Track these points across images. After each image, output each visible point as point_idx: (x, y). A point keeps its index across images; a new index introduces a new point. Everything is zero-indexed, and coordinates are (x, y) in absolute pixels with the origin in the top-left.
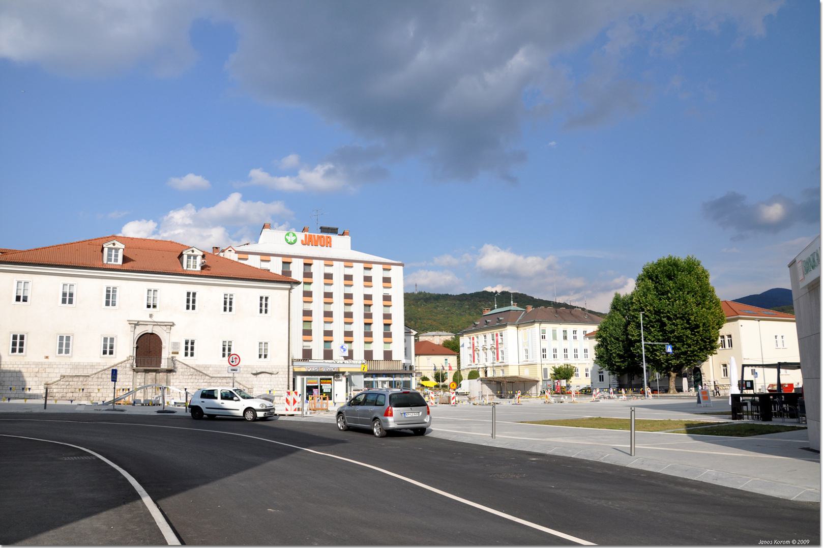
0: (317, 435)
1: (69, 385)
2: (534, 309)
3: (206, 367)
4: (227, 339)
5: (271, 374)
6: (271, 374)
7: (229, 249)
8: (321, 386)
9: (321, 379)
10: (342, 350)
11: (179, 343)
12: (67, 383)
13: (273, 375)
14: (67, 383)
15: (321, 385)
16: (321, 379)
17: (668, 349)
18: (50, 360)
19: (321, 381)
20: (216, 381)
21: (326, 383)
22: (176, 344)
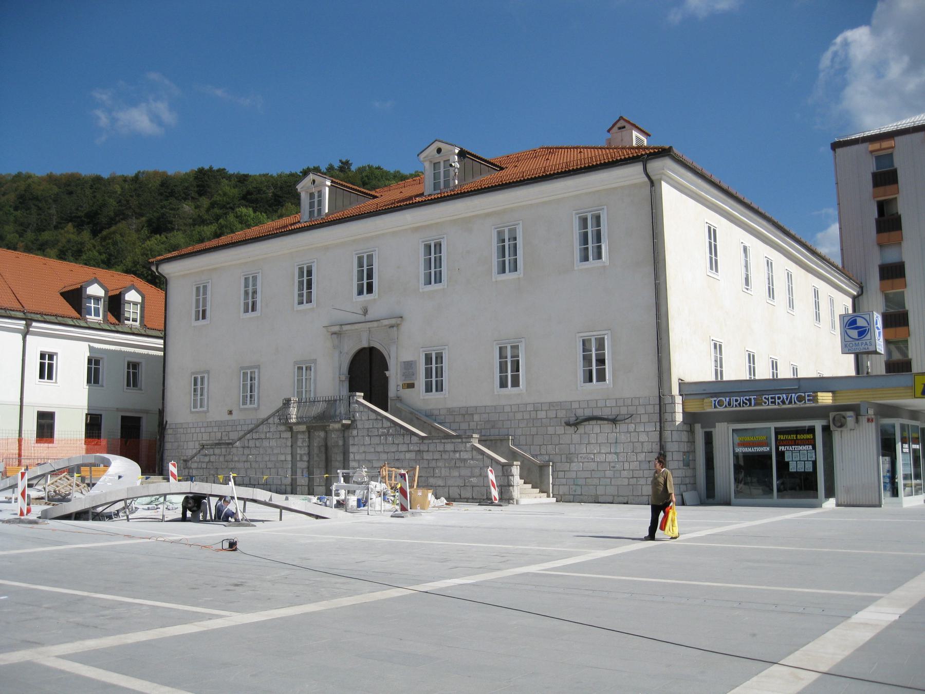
0: (17, 661)
1: (210, 461)
2: (301, 174)
3: (467, 414)
4: (593, 335)
5: (614, 421)
6: (614, 421)
7: (619, 125)
8: (781, 455)
9: (778, 432)
10: (854, 333)
11: (415, 362)
12: (207, 459)
13: (622, 427)
14: (207, 459)
15: (782, 448)
16: (778, 432)
17: (350, 441)
18: (235, 416)
19: (781, 437)
20: (841, 456)
21: (795, 443)
22: (409, 367)
